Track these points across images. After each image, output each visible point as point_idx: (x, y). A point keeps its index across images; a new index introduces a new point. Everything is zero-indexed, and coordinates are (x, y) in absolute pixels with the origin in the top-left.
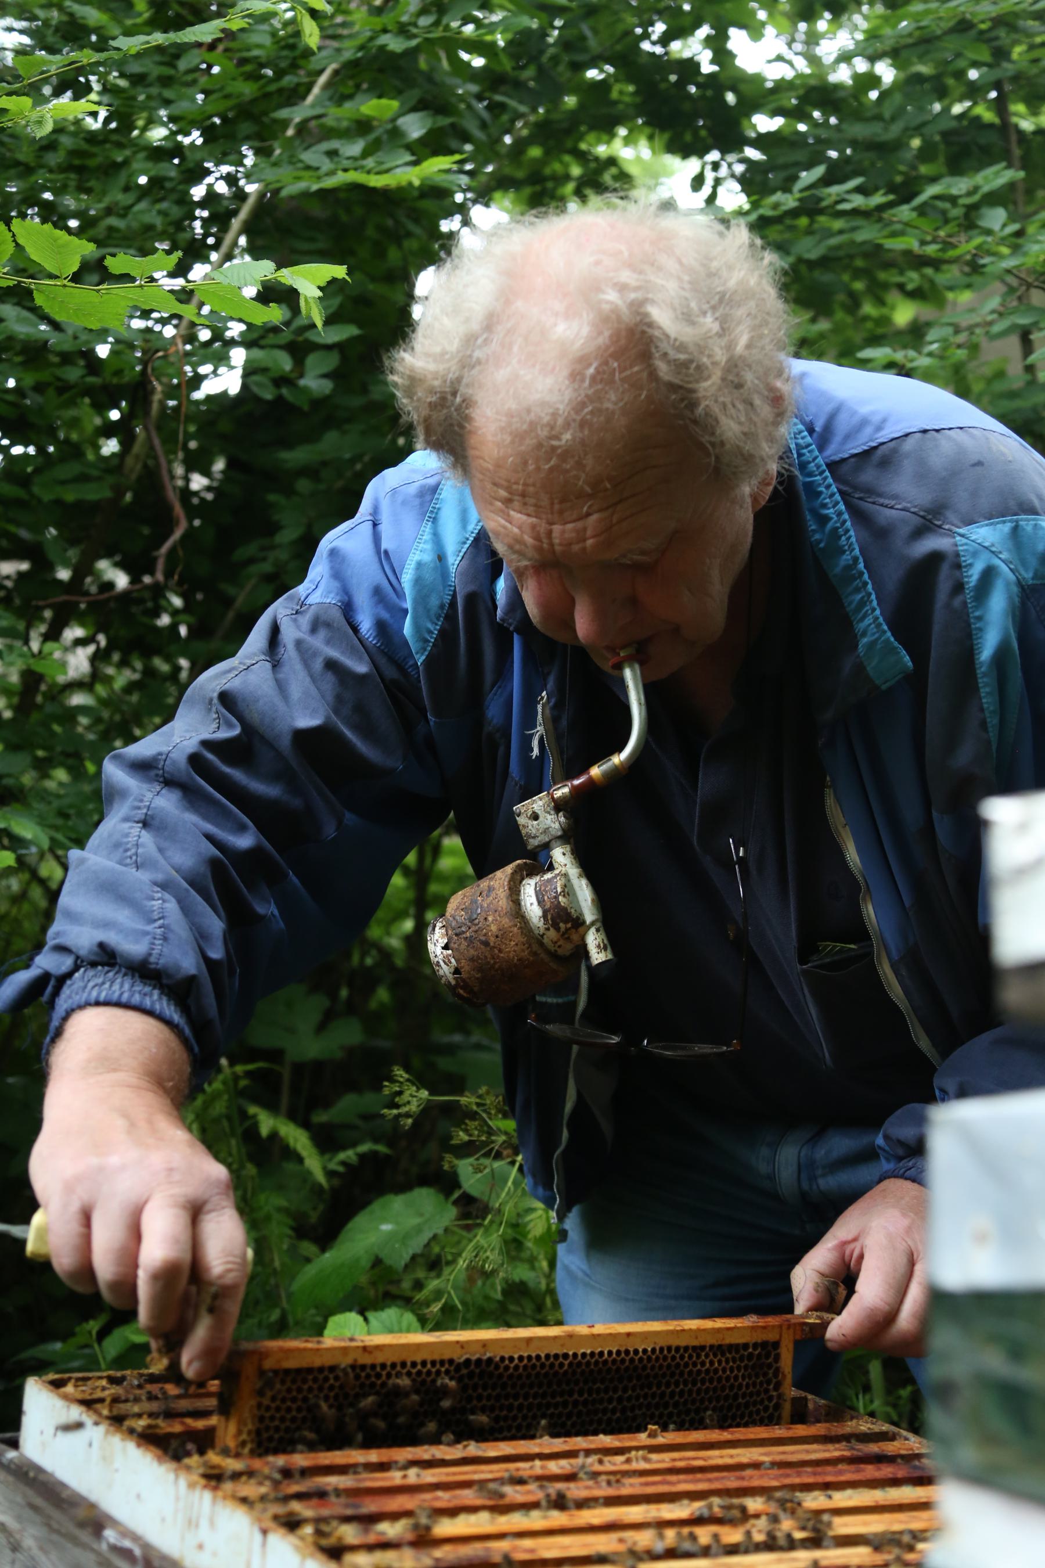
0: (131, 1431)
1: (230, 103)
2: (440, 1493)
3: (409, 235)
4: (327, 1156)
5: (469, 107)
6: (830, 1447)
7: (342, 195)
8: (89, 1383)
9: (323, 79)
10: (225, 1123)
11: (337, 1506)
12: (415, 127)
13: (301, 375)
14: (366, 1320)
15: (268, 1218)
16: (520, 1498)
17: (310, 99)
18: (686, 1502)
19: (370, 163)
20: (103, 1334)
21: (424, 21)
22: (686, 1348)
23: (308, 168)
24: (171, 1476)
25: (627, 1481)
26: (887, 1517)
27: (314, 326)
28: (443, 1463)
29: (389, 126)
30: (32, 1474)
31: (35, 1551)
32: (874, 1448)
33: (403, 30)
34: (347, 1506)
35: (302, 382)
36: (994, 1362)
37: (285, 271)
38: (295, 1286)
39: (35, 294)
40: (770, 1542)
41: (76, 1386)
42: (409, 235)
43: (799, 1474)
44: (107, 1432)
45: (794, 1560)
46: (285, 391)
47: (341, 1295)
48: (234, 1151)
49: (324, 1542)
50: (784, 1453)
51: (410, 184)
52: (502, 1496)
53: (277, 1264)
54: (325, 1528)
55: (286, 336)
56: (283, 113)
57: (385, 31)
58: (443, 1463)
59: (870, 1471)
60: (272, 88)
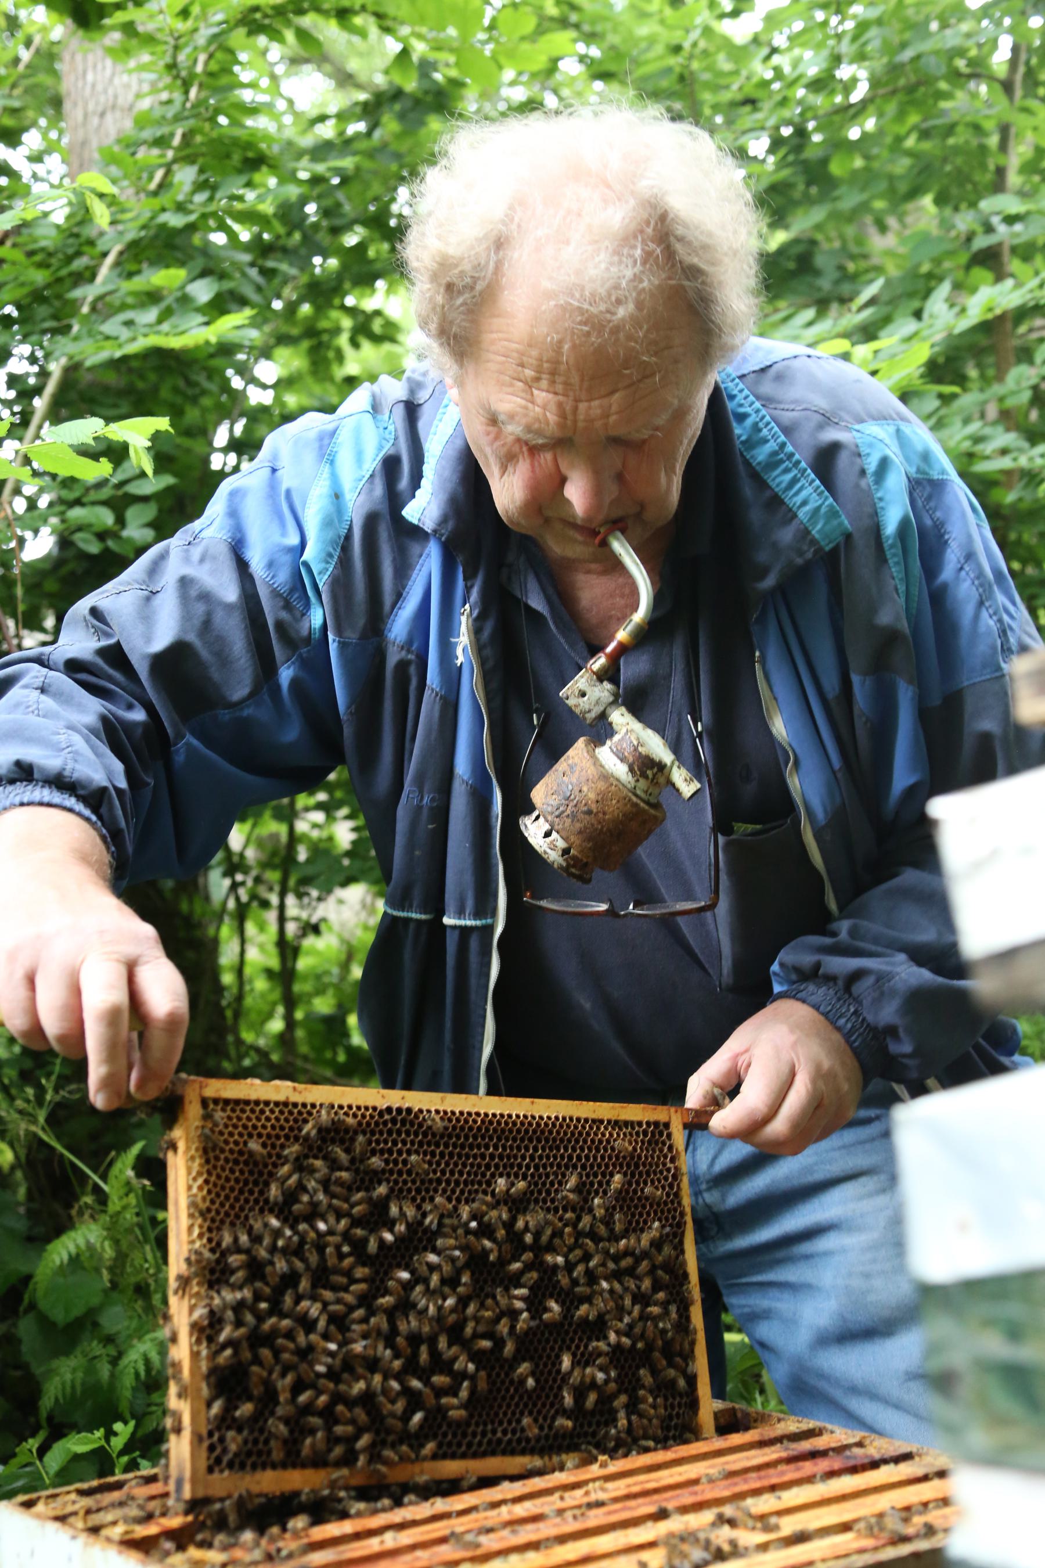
0: (109, 1540)
1: (25, 291)
2: (419, 1553)
3: (204, 392)
5: (244, 275)
6: (767, 1450)
7: (135, 364)
9: (110, 260)
12: (203, 291)
16: (496, 1546)
17: (99, 279)
18: (650, 1524)
19: (165, 327)
20: (42, 1451)
21: (200, 198)
22: (586, 1120)
23: (108, 338)
26: (834, 1508)
27: (143, 474)
28: (414, 1523)
29: (179, 294)
32: (806, 1445)
33: (181, 208)
35: (125, 533)
36: (995, 1346)
37: (114, 426)
42: (204, 392)
43: (746, 1481)
44: (86, 1544)
45: (761, 1564)
46: (111, 543)
48: (150, 1257)
51: (207, 343)
52: (478, 1546)
55: (106, 493)
56: (77, 293)
57: (164, 210)
58: (414, 1523)
59: (808, 1468)
60: (64, 272)
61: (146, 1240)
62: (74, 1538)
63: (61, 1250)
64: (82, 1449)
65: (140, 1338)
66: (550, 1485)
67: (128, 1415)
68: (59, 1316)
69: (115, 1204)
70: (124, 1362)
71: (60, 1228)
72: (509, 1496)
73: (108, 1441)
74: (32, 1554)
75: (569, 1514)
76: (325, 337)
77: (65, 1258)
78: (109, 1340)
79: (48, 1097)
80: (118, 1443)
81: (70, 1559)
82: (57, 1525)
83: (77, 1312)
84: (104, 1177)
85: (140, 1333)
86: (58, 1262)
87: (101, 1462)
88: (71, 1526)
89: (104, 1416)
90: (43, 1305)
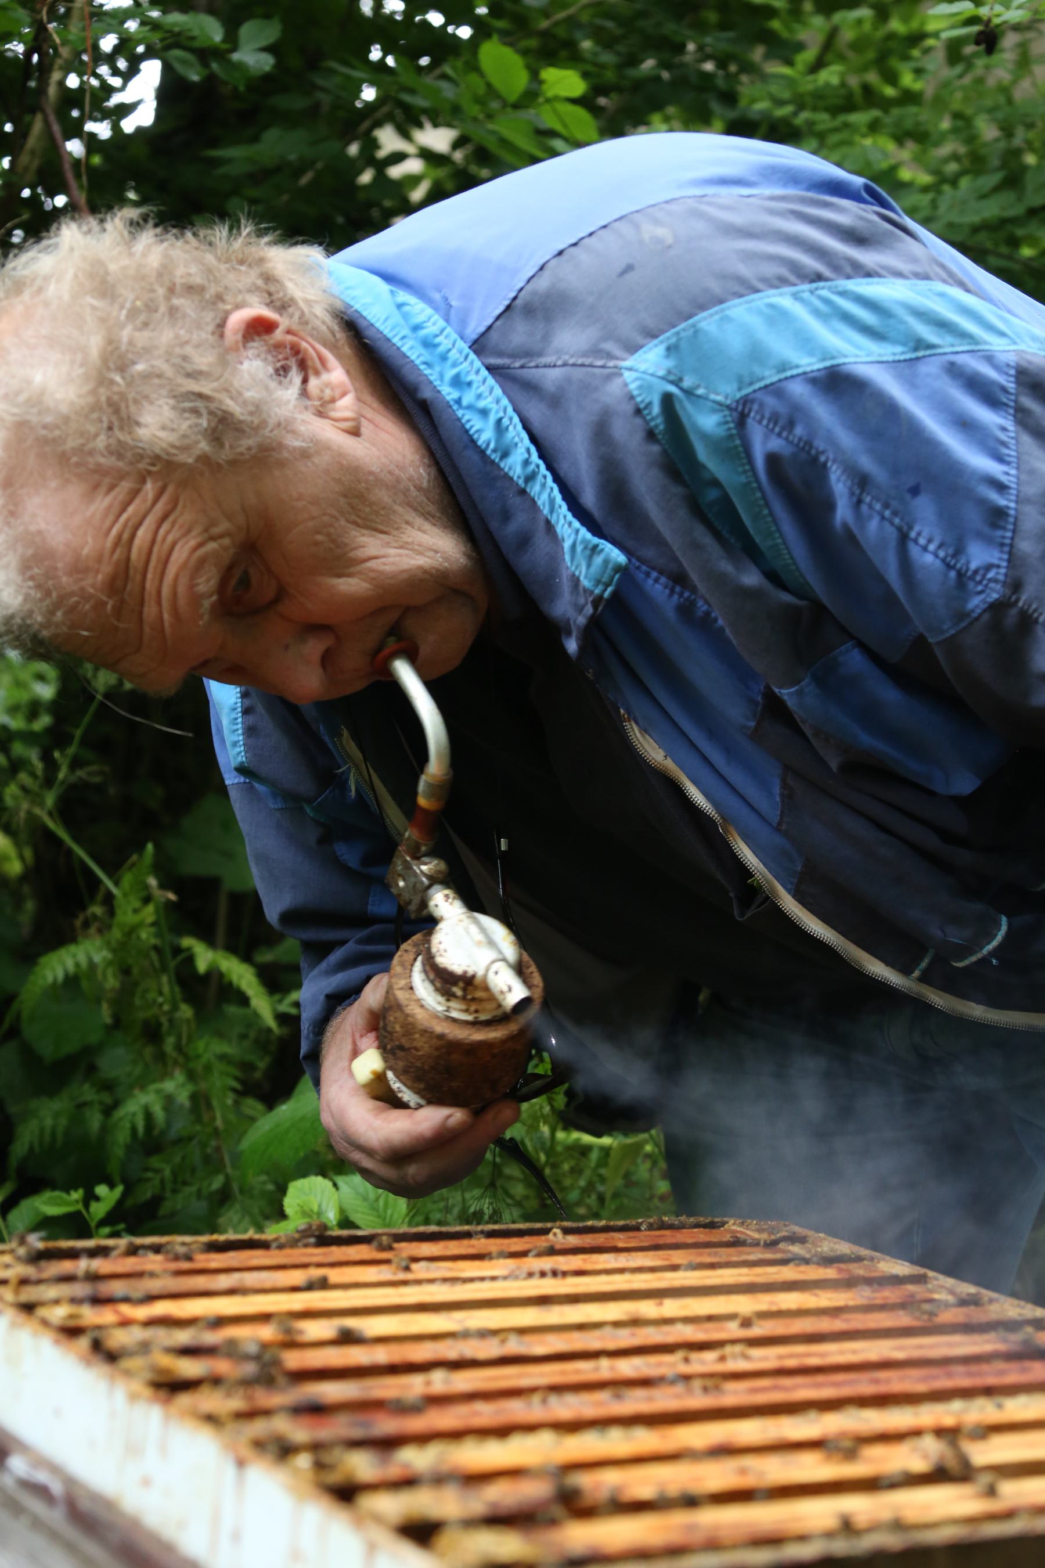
0: (45, 1323)
4: (277, 997)
6: (977, 1338)
10: (154, 956)
11: (339, 1427)
13: (234, 49)
14: (335, 1185)
15: (208, 1068)
25: (731, 1386)
35: (236, 57)
38: (245, 1144)
40: (288, 1338)
43: (950, 1375)
44: (13, 1325)
47: (302, 1154)
48: (166, 989)
49: (334, 1478)
50: (920, 1347)
53: (219, 1123)
54: (327, 1458)
61: (164, 969)
63: (57, 965)
65: (143, 1087)
67: (117, 1177)
68: (47, 1050)
70: (120, 1113)
71: (55, 934)
72: (611, 1345)
73: (87, 1206)
75: (697, 1384)
77: (60, 976)
78: (108, 1086)
79: (61, 775)
80: (99, 1210)
83: (70, 1047)
84: (117, 884)
85: (142, 1083)
86: (50, 979)
89: (87, 1175)
90: (30, 1031)
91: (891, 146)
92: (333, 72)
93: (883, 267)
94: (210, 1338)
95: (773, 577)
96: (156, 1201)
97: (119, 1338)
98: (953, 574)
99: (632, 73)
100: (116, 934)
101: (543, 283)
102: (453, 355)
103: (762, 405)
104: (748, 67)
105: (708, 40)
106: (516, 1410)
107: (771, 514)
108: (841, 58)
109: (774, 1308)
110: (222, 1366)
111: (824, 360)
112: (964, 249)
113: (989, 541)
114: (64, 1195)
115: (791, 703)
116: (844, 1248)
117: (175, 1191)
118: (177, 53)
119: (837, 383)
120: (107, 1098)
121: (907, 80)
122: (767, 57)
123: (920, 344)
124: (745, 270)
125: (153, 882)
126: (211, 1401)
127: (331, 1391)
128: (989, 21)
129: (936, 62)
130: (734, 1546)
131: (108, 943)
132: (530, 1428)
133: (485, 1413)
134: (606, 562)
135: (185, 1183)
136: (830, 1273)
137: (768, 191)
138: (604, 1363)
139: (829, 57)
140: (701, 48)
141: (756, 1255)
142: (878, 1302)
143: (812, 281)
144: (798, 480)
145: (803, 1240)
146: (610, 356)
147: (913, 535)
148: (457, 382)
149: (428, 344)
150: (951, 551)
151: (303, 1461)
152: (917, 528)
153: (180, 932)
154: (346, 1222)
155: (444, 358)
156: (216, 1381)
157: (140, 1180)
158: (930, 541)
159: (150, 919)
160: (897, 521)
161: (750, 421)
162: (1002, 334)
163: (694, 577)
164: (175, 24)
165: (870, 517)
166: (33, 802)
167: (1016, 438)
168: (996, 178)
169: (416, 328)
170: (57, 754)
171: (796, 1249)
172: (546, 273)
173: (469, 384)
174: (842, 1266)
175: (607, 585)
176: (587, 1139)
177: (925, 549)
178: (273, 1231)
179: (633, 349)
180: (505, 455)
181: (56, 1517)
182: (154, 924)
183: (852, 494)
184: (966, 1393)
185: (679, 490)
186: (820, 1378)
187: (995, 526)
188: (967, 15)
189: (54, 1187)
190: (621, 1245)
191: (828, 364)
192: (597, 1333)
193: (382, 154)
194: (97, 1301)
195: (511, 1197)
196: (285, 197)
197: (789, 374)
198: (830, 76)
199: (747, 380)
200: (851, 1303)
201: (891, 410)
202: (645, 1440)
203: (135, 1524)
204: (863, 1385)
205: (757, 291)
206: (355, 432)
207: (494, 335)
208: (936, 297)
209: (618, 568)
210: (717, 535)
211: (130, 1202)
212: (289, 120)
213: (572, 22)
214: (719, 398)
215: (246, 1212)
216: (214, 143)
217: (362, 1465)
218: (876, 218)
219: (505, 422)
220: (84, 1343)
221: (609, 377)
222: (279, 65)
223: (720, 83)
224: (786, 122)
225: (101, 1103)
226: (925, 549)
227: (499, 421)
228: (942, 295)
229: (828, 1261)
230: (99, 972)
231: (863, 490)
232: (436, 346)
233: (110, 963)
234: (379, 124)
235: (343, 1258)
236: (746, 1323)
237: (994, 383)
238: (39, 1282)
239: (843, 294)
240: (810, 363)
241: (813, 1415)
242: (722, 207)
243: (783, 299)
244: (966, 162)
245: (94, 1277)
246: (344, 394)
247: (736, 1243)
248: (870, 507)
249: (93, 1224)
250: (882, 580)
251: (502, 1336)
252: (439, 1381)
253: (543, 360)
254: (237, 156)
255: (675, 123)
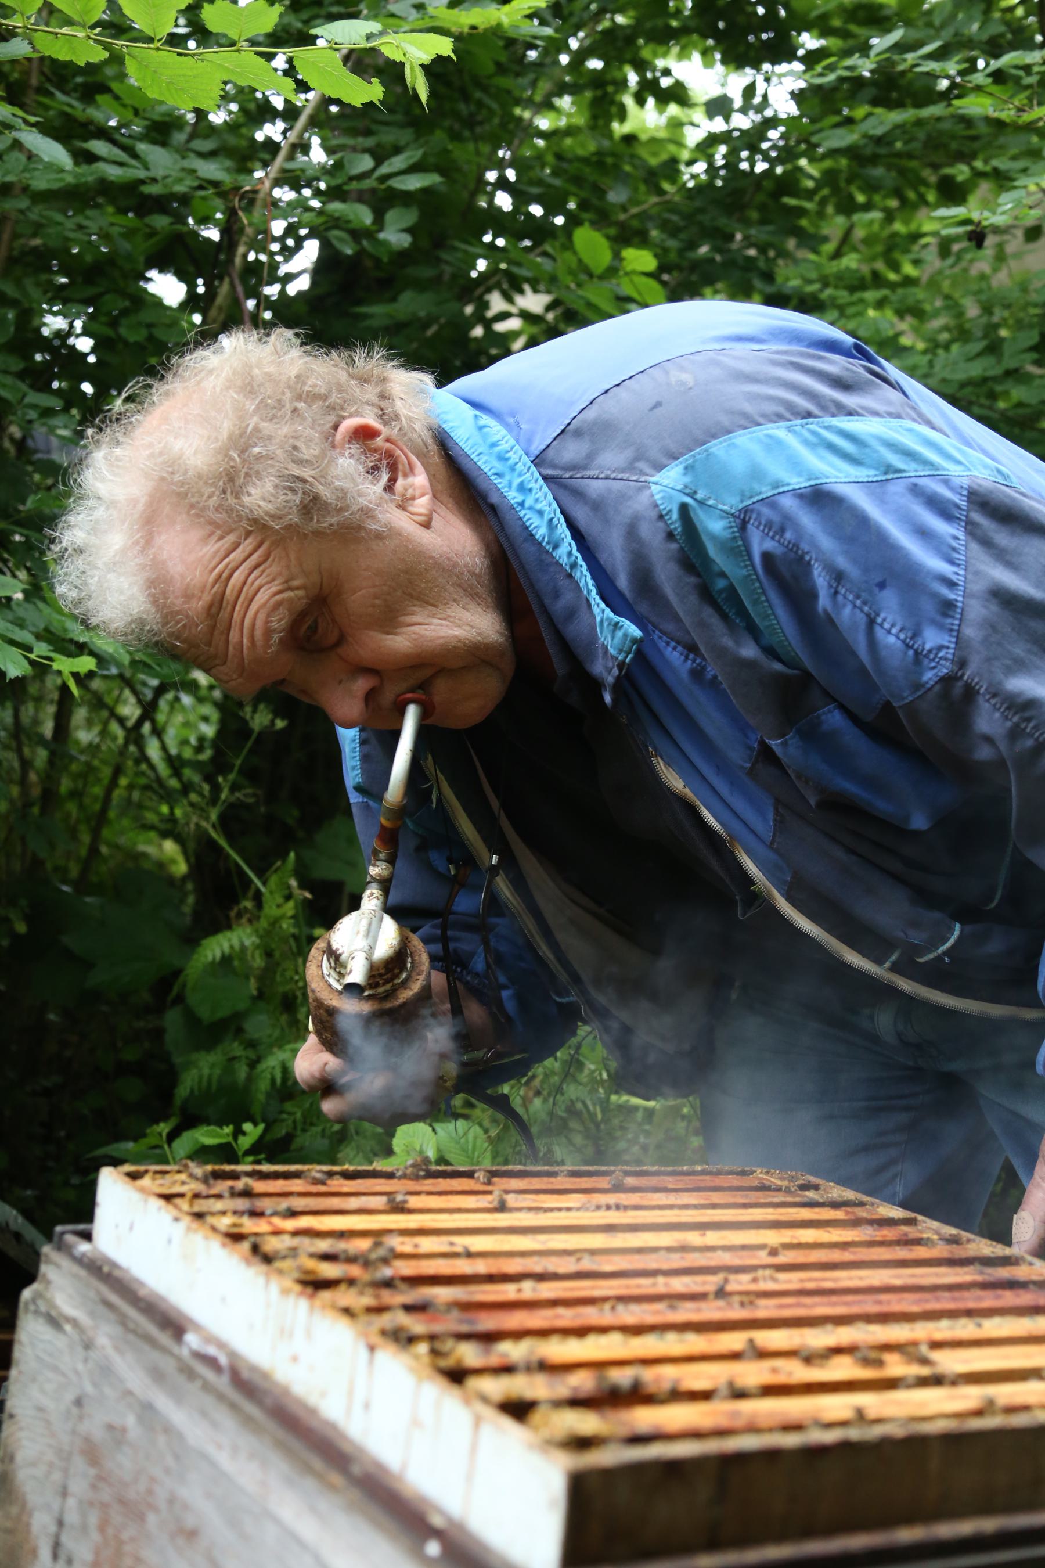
0: (214, 1229)
6: (959, 1270)
8: (167, 1176)
10: (292, 942)
13: (381, 229)
14: (434, 1130)
20: (172, 1136)
24: (261, 1280)
25: (762, 1302)
28: (555, 1277)
30: (106, 1269)
31: (110, 1351)
32: (1003, 1273)
34: (461, 1321)
35: (382, 236)
39: (128, 61)
41: (154, 1179)
43: (938, 1299)
44: (189, 1229)
49: (444, 1363)
50: (913, 1276)
54: (438, 1345)
62: (177, 1219)
63: (216, 947)
64: (209, 1141)
65: (280, 1047)
66: (713, 1263)
67: (258, 1118)
68: (205, 1013)
69: (271, 909)
71: (219, 925)
72: (665, 1266)
73: (235, 1138)
74: (131, 1228)
76: (610, 89)
77: (218, 955)
78: (252, 1044)
79: (223, 796)
80: (245, 1142)
81: (170, 1241)
82: (161, 1203)
83: (223, 1013)
84: (264, 883)
86: (210, 958)
87: (226, 1153)
88: (176, 1206)
89: (236, 1114)
90: (193, 999)
91: (895, 319)
92: (455, 249)
93: (862, 408)
94: (341, 1246)
95: (770, 651)
96: (289, 1138)
97: (272, 1244)
98: (911, 652)
99: (691, 255)
100: (263, 923)
101: (591, 414)
102: (519, 467)
103: (759, 514)
104: (783, 253)
105: (753, 232)
106: (590, 1315)
107: (767, 600)
108: (855, 249)
109: (795, 1241)
110: (355, 1271)
111: (809, 480)
112: (953, 400)
113: (941, 627)
114: (218, 1129)
115: (778, 751)
116: (850, 1194)
117: (304, 1130)
118: (336, 233)
119: (819, 498)
120: (251, 1054)
121: (908, 269)
122: (799, 246)
123: (889, 469)
124: (749, 408)
125: (293, 883)
126: (346, 1297)
127: (443, 1294)
128: (979, 223)
129: (931, 256)
130: (771, 1430)
131: (257, 931)
132: (603, 1330)
133: (566, 1317)
134: (625, 635)
135: (312, 1124)
136: (839, 1214)
137: (774, 347)
138: (661, 1280)
139: (845, 249)
140: (746, 238)
141: (779, 1198)
142: (878, 1239)
143: (804, 418)
144: (787, 573)
145: (816, 1188)
146: (642, 473)
147: (879, 620)
148: (522, 488)
149: (502, 458)
150: (910, 634)
151: (423, 1348)
152: (882, 615)
153: (312, 925)
154: (442, 1160)
155: (513, 469)
156: (351, 1282)
157: (275, 1121)
158: (893, 626)
159: (290, 913)
160: (866, 609)
161: (749, 526)
162: (959, 463)
163: (702, 648)
164: (336, 211)
165: (844, 606)
166: (201, 816)
167: (966, 546)
168: (978, 346)
169: (494, 445)
170: (220, 779)
171: (811, 1194)
172: (594, 406)
173: (530, 490)
174: (849, 1209)
175: (628, 653)
176: (635, 1101)
177: (889, 632)
178: (380, 1165)
179: (659, 467)
180: (556, 547)
181: (223, 1382)
182: (293, 917)
183: (831, 586)
184: (952, 1314)
185: (692, 580)
186: (834, 1299)
187: (945, 615)
188: (962, 217)
189: (208, 1122)
190: (670, 1186)
191: (813, 483)
192: (654, 1256)
193: (490, 314)
194: (255, 1214)
195: (574, 1145)
196: (415, 345)
197: (781, 490)
198: (850, 261)
199: (748, 494)
200: (857, 1239)
201: (863, 521)
202: (695, 1343)
203: (286, 1391)
204: (870, 1305)
205: (759, 424)
206: (427, 525)
207: (551, 453)
208: (904, 432)
209: (635, 641)
210: (724, 617)
211: (268, 1137)
212: (421, 286)
213: (643, 216)
214: (725, 508)
215: (359, 1149)
216: (359, 302)
217: (469, 1354)
218: (862, 371)
219: (555, 521)
220: (246, 1246)
221: (640, 489)
222: (414, 244)
223: (762, 264)
224: (814, 296)
225: (247, 1058)
226: (889, 632)
227: (551, 520)
228: (910, 430)
229: (835, 1205)
230: (249, 953)
231: (839, 583)
232: (507, 459)
233: (258, 947)
234: (489, 290)
235: (449, 1189)
236: (774, 1252)
237: (949, 501)
238: (208, 1197)
239: (828, 428)
240: (798, 482)
241: (829, 1327)
242: (735, 358)
243: (778, 431)
244: (955, 333)
245: (247, 1193)
246: (423, 495)
247: (764, 1188)
248: (845, 597)
249: (240, 1154)
250: (853, 654)
251: (578, 1255)
252: (528, 1290)
253: (588, 473)
254: (378, 311)
255: (722, 296)
